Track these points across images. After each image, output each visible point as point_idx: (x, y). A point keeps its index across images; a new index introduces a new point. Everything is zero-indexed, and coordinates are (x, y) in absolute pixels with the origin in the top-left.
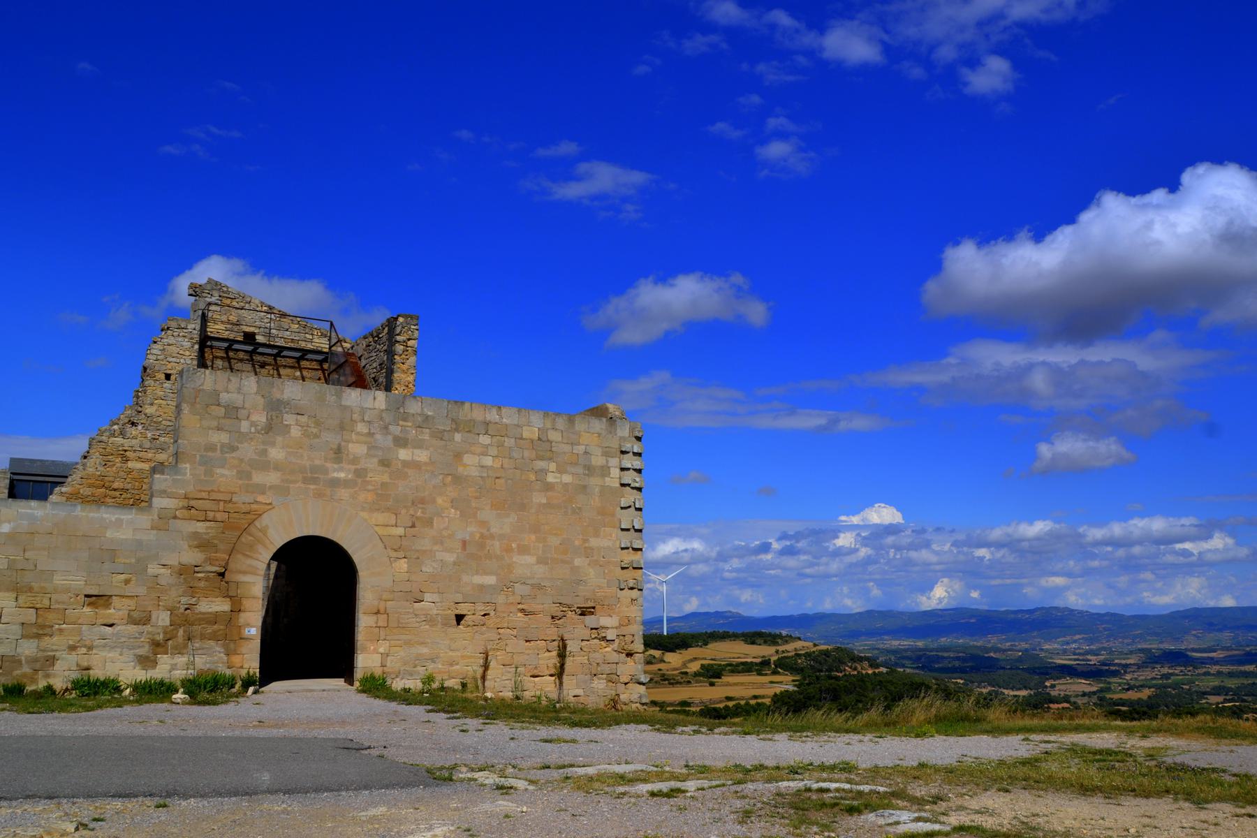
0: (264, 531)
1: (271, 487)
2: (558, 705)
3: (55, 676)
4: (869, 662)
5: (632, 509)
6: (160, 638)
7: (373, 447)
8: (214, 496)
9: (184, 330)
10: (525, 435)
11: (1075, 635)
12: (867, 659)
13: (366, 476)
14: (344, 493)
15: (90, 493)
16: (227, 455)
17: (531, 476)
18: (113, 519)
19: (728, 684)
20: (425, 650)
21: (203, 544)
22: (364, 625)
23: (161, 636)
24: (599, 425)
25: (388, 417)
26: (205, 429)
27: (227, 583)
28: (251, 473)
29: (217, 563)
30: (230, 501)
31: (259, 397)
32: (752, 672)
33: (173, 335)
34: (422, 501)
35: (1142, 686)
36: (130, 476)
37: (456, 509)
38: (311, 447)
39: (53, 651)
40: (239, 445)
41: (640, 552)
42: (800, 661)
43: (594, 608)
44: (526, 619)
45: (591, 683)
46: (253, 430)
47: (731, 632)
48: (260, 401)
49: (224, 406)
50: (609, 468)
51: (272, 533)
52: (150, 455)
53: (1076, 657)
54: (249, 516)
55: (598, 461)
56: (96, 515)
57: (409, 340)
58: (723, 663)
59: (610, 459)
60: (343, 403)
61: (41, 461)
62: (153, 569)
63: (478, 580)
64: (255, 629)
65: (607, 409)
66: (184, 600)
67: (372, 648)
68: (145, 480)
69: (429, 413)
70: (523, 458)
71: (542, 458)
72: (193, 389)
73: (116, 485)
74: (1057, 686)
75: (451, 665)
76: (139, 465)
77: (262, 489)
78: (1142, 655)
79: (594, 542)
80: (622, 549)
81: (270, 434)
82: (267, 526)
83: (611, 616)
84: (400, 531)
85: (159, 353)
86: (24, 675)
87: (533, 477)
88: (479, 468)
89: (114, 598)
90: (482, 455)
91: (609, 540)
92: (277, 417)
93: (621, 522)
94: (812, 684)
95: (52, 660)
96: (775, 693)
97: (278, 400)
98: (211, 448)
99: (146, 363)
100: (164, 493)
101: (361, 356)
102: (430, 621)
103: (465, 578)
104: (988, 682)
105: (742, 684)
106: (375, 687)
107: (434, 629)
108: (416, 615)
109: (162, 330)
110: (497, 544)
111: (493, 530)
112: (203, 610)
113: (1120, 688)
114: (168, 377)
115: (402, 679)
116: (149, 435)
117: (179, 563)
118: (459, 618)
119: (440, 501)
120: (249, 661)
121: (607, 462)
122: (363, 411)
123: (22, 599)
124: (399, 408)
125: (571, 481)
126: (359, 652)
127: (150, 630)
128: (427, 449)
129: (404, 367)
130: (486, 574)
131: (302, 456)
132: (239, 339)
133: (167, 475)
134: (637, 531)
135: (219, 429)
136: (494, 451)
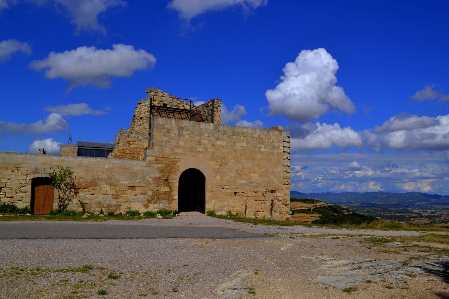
0: (178, 167)
1: (180, 153)
2: (271, 220)
3: (121, 210)
4: (346, 210)
5: (287, 159)
6: (150, 199)
7: (210, 141)
8: (164, 156)
9: (146, 104)
10: (255, 136)
11: (422, 202)
12: (345, 209)
13: (208, 150)
14: (201, 155)
15: (120, 155)
16: (167, 144)
17: (256, 149)
18: (136, 164)
19: (296, 217)
20: (226, 203)
21: (161, 171)
22: (208, 195)
23: (150, 198)
24: (277, 133)
25: (214, 131)
26: (161, 136)
27: (168, 183)
28: (174, 149)
29: (165, 177)
30: (169, 158)
31: (176, 126)
32: (304, 213)
33: (142, 105)
34: (224, 157)
35: (447, 221)
36: (131, 149)
37: (234, 160)
38: (192, 141)
39: (121, 203)
40: (171, 141)
41: (289, 173)
42: (321, 209)
43: (275, 190)
44: (255, 194)
45: (274, 214)
46: (174, 136)
47: (297, 198)
48: (176, 127)
49: (166, 129)
50: (280, 146)
51: (181, 167)
52: (137, 143)
53: (423, 210)
54: (174, 162)
55: (276, 144)
56: (131, 162)
57: (218, 107)
58: (294, 209)
59: (280, 144)
60: (200, 127)
61: (86, 142)
62: (147, 178)
63: (241, 182)
64: (176, 196)
65: (278, 127)
66: (156, 188)
67: (210, 202)
68: (136, 151)
69: (226, 130)
70: (254, 144)
71: (259, 144)
72: (157, 124)
73: (127, 152)
74: (415, 220)
75: (233, 208)
76: (134, 146)
77: (177, 154)
78: (448, 210)
79: (275, 170)
80: (284, 172)
81: (180, 137)
82: (179, 165)
83: (281, 193)
84: (218, 167)
85: (138, 111)
86: (113, 210)
87: (257, 150)
88: (241, 147)
89: (137, 187)
90: (242, 143)
91: (280, 169)
92: (181, 132)
93: (283, 164)
94: (326, 217)
95: (120, 205)
96: (313, 220)
97: (181, 127)
98: (162, 142)
99: (135, 114)
100: (150, 156)
101: (201, 111)
102: (227, 194)
103: (237, 181)
104: (389, 218)
105: (301, 217)
106: (212, 214)
107: (228, 197)
108: (223, 192)
109: (138, 104)
110: (247, 170)
111: (245, 166)
112: (162, 191)
113: (439, 222)
114: (141, 118)
115: (219, 212)
116: (136, 137)
117: (155, 177)
118: (235, 193)
119: (229, 157)
120: (175, 206)
121: (279, 145)
122: (206, 129)
123: (112, 187)
124: (217, 129)
125: (268, 151)
126: (206, 204)
127: (147, 197)
128: (226, 141)
129: (217, 115)
130: (244, 180)
131: (189, 144)
132: (162, 106)
133: (150, 150)
134: (288, 166)
135: (165, 136)
136: (245, 142)
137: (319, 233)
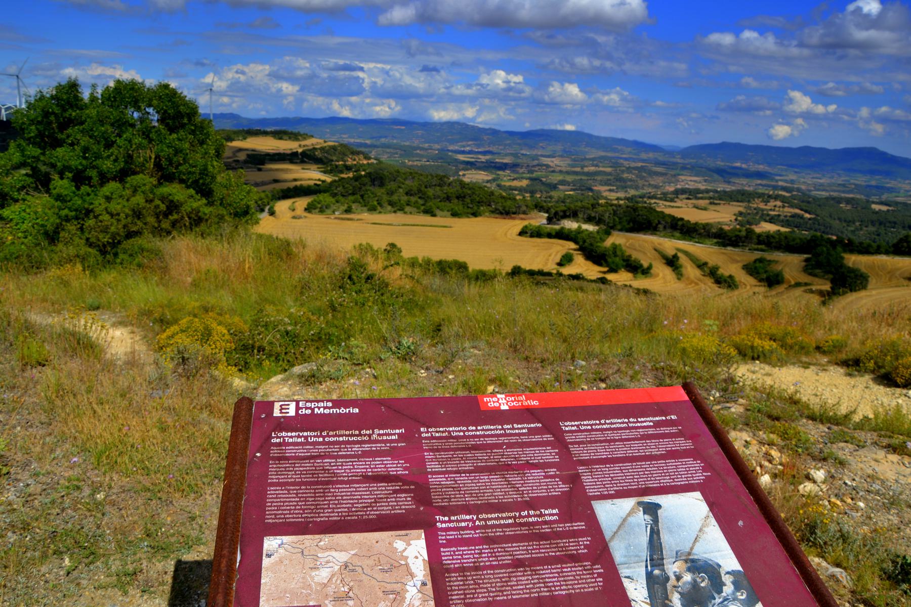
137: (334, 141)
